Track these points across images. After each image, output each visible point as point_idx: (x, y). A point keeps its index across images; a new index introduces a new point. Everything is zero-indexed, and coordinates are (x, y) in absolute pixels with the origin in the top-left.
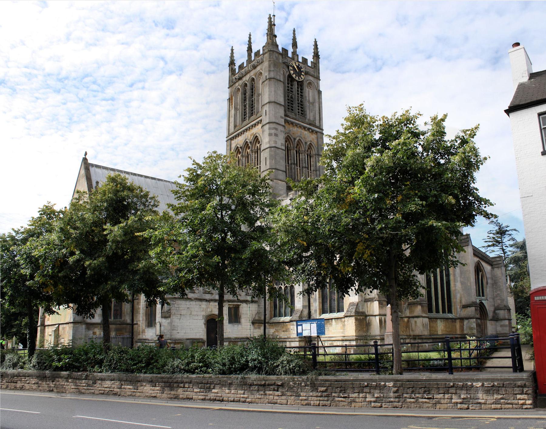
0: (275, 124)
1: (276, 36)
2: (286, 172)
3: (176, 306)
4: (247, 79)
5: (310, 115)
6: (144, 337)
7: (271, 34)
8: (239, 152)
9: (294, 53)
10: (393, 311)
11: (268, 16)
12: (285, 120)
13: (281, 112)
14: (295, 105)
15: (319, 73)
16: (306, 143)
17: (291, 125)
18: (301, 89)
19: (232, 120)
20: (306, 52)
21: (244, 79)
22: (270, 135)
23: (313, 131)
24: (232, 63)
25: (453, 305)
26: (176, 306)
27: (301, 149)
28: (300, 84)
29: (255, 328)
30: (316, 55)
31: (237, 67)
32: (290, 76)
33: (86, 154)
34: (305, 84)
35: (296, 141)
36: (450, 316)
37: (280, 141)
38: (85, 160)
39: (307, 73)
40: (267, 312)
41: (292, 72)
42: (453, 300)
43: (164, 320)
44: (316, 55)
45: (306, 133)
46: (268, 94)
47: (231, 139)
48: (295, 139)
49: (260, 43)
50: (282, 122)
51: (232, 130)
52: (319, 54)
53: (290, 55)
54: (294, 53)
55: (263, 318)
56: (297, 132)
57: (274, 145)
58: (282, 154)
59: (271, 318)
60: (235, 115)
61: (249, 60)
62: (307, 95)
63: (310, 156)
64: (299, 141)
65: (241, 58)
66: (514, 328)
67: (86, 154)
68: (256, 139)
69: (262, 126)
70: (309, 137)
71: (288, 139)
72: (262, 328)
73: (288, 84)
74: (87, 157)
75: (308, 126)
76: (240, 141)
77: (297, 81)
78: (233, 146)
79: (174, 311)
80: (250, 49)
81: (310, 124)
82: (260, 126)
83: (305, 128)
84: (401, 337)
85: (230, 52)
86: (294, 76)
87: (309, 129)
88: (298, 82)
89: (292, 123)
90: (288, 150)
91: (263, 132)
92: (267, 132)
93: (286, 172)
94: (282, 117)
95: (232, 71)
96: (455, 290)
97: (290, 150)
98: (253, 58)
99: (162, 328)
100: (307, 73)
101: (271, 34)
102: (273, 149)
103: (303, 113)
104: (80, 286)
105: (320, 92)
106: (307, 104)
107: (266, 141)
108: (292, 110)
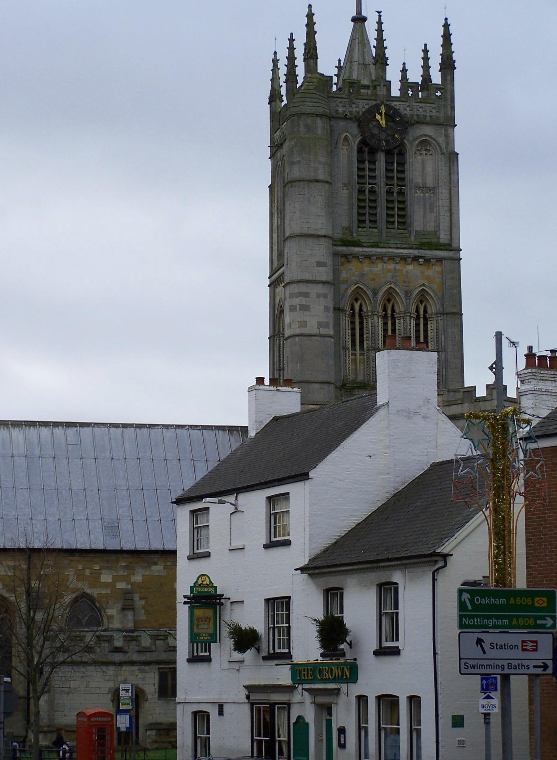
0: (295, 285)
3: (60, 674)
5: (420, 220)
10: (170, 641)
15: (453, 108)
16: (408, 294)
17: (367, 261)
18: (402, 164)
21: (65, 461)
23: (427, 261)
26: (60, 674)
27: (397, 310)
35: (381, 294)
44: (448, 65)
48: (375, 293)
52: (455, 57)
57: (298, 331)
66: (129, 648)
75: (416, 252)
79: (58, 683)
81: (421, 246)
83: (404, 259)
84: (271, 651)
85: (305, 20)
87: (416, 259)
89: (368, 257)
97: (367, 319)
102: (297, 339)
104: (61, 630)
105: (453, 157)
106: (414, 198)
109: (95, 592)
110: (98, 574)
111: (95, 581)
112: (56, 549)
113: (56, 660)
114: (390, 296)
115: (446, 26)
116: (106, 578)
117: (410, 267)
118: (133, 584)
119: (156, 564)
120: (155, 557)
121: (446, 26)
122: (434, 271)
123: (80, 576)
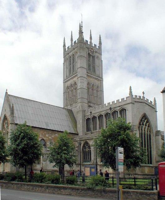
1: (83, 33)
2: (87, 99)
4: (71, 54)
5: (97, 72)
6: (36, 168)
7: (81, 32)
8: (68, 88)
9: (91, 42)
11: (79, 24)
12: (87, 75)
13: (85, 71)
14: (91, 68)
19: (65, 73)
20: (95, 42)
21: (70, 54)
22: (81, 82)
24: (64, 46)
25: (152, 160)
28: (93, 57)
29: (77, 167)
30: (100, 43)
31: (66, 48)
32: (89, 54)
33: (7, 90)
34: (96, 57)
36: (151, 165)
37: (85, 85)
38: (6, 93)
39: (96, 52)
40: (81, 160)
41: (90, 52)
42: (152, 159)
43: (44, 162)
45: (96, 81)
46: (81, 63)
47: (65, 82)
48: (91, 84)
49: (76, 37)
50: (86, 76)
51: (65, 78)
53: (89, 43)
54: (91, 42)
55: (80, 163)
56: (92, 81)
58: (86, 91)
59: (83, 163)
60: (67, 72)
61: (72, 45)
62: (96, 63)
63: (97, 91)
64: (93, 85)
65: (68, 44)
67: (7, 90)
68: (75, 83)
69: (78, 78)
70: (97, 83)
71: (88, 84)
72: (79, 167)
73: (88, 57)
74: (7, 91)
75: (97, 78)
76: (69, 83)
77: (92, 56)
78: (66, 86)
80: (72, 40)
82: (77, 77)
85: (64, 40)
86: (91, 53)
88: (92, 56)
89: (90, 76)
90: (88, 88)
91: (78, 81)
92: (79, 81)
93: (87, 99)
94: (85, 74)
95: (65, 49)
96: (153, 155)
98: (73, 45)
99: (43, 165)
100: (96, 52)
101: (81, 32)
103: (94, 71)
105: (102, 61)
107: (79, 85)
108: (90, 70)
109: (45, 139)
110: (45, 134)
111: (45, 136)
112: (100, 79)
113: (139, 149)
114: (93, 84)
115: (100, 36)
116: (47, 136)
117: (96, 80)
118: (52, 138)
119: (56, 134)
120: (56, 132)
121: (100, 36)
122: (99, 82)
123: (42, 135)
